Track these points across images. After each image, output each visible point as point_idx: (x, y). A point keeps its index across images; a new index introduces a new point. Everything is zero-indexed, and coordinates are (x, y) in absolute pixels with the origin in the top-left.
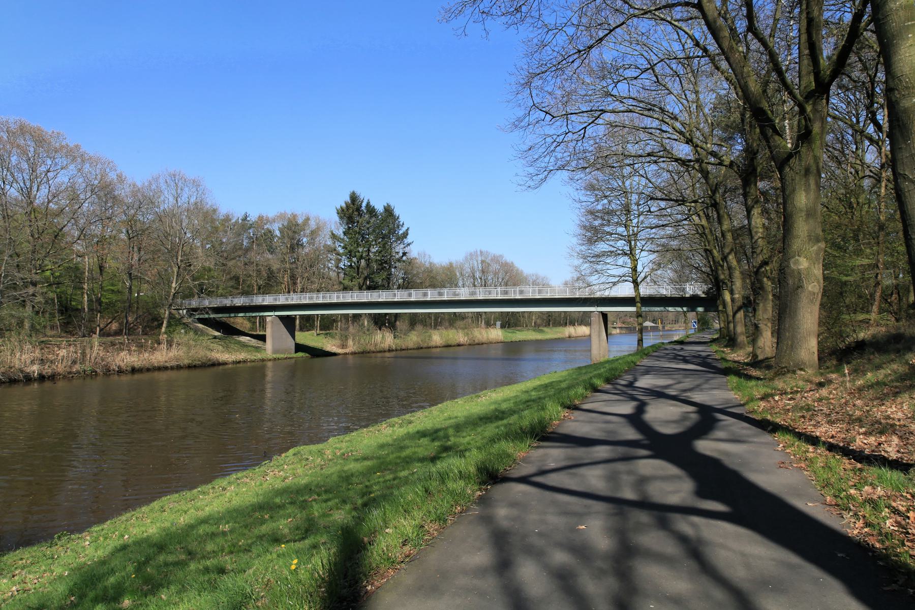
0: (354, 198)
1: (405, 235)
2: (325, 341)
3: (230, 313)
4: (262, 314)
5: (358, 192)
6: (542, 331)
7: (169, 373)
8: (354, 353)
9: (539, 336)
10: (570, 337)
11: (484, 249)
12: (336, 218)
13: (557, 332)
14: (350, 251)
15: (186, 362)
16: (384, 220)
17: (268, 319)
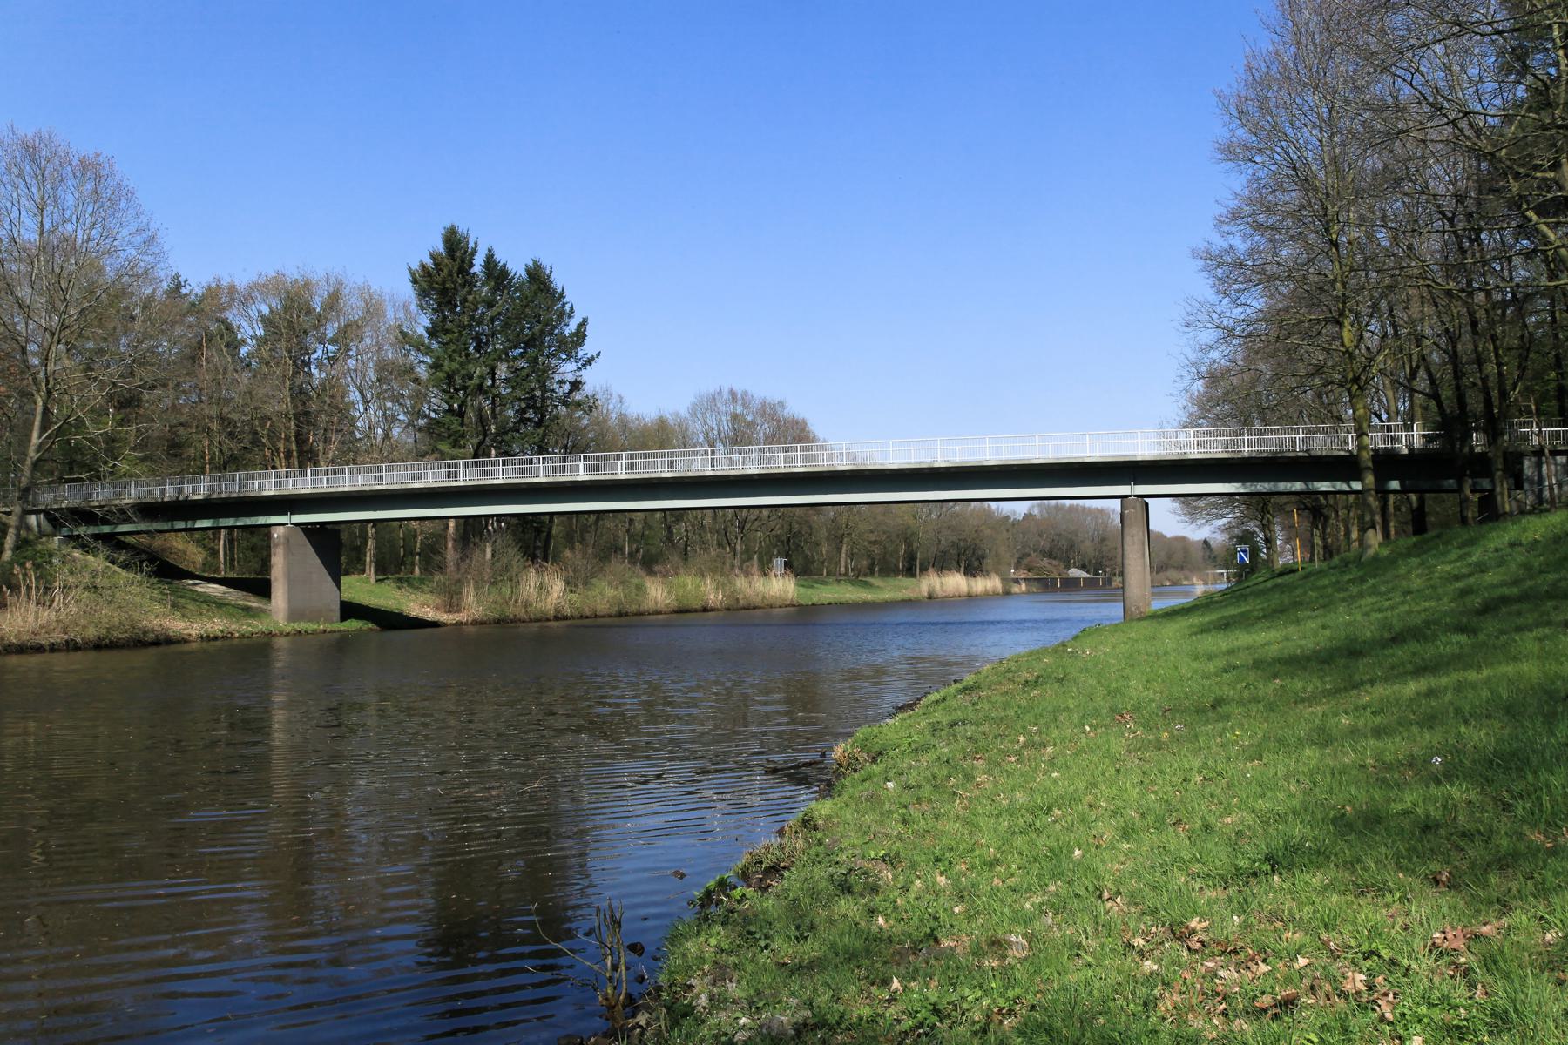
0: (454, 242)
1: (580, 336)
2: (397, 594)
3: (172, 518)
4: (261, 520)
5: (462, 228)
6: (867, 585)
7: (46, 657)
8: (475, 623)
9: (867, 595)
10: (930, 597)
11: (738, 388)
12: (407, 292)
13: (900, 588)
14: (450, 377)
15: (91, 633)
16: (527, 301)
17: (277, 533)
